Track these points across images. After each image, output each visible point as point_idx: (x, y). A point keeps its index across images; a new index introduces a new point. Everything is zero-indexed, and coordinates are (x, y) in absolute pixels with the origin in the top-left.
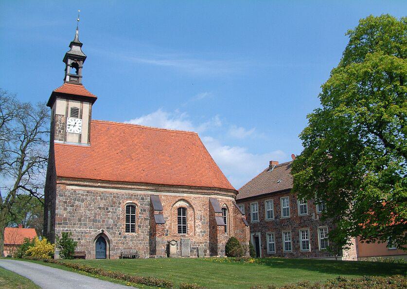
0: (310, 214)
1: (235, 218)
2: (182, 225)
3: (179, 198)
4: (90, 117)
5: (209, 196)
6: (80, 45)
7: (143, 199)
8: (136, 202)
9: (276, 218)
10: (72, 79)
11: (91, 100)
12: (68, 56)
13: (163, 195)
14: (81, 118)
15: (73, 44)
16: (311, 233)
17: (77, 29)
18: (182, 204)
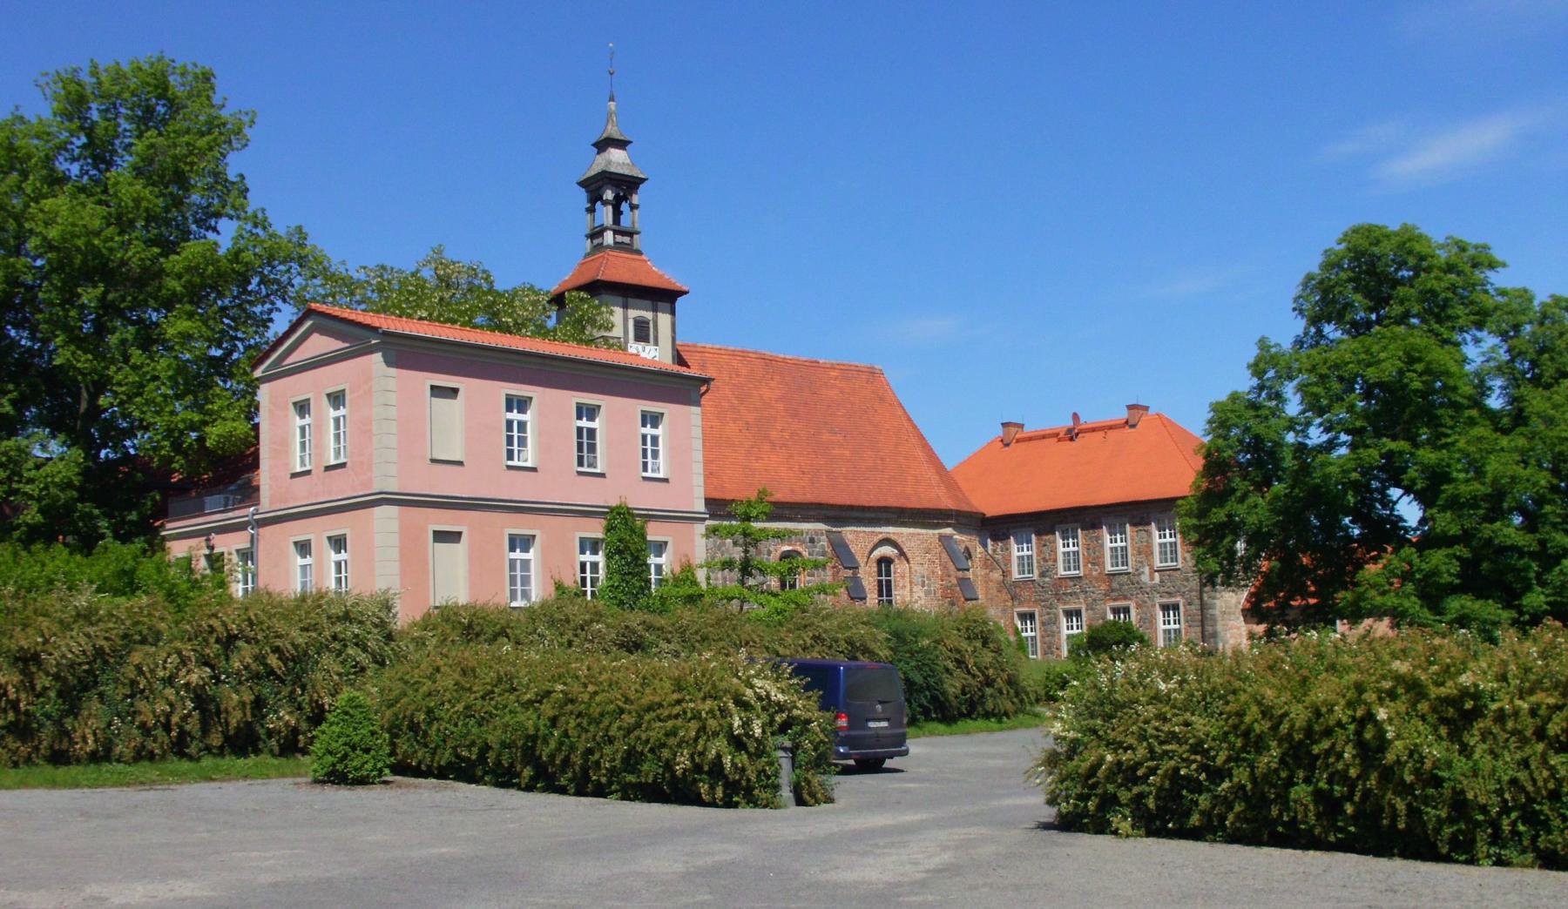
0: (1137, 570)
1: (987, 580)
2: (885, 598)
3: (880, 536)
4: (674, 339)
5: (937, 531)
6: (622, 144)
7: (812, 541)
8: (799, 549)
9: (1042, 575)
10: (619, 238)
11: (664, 297)
12: (594, 186)
13: (849, 533)
14: (656, 343)
15: (603, 145)
16: (1137, 614)
17: (612, 99)
18: (887, 551)
